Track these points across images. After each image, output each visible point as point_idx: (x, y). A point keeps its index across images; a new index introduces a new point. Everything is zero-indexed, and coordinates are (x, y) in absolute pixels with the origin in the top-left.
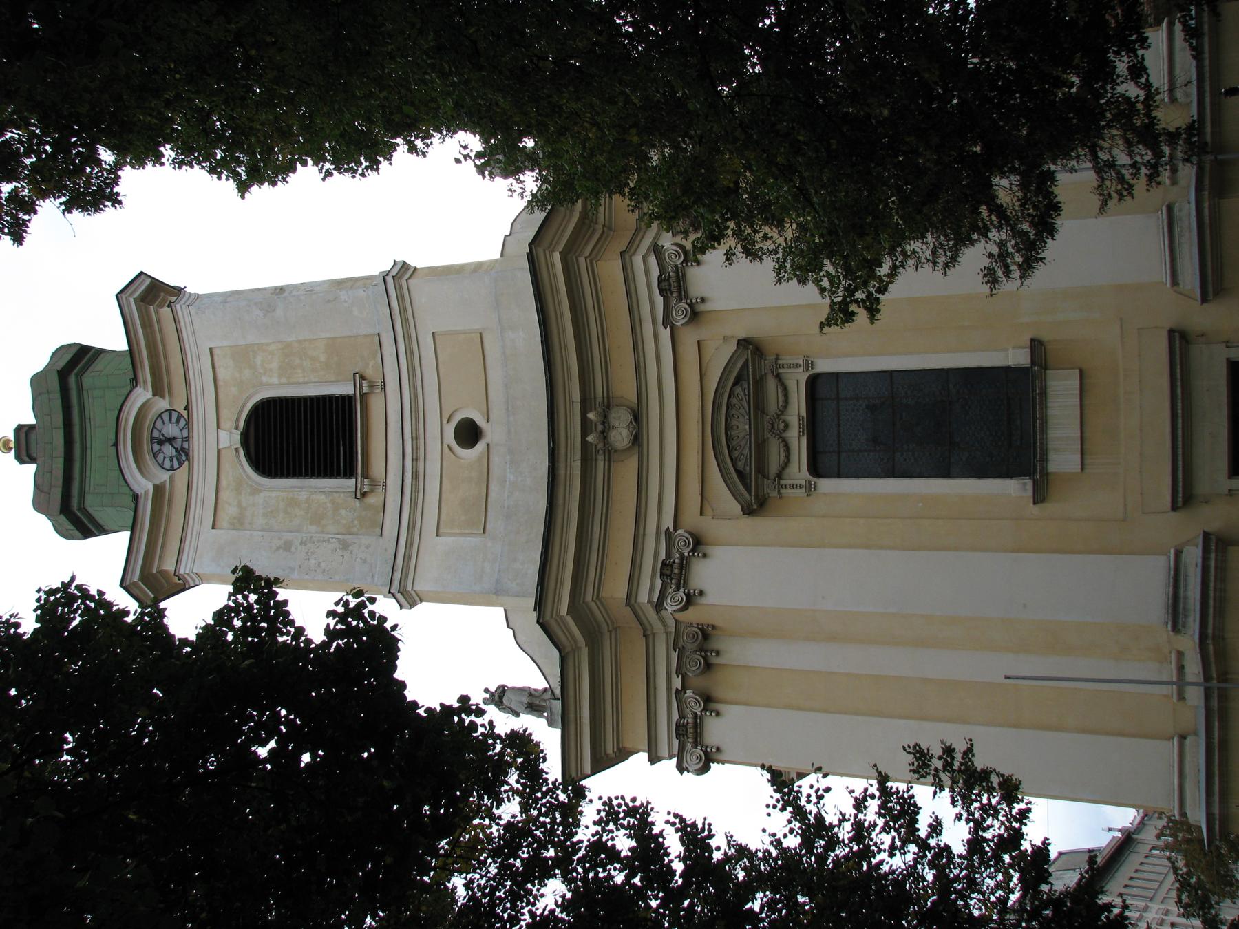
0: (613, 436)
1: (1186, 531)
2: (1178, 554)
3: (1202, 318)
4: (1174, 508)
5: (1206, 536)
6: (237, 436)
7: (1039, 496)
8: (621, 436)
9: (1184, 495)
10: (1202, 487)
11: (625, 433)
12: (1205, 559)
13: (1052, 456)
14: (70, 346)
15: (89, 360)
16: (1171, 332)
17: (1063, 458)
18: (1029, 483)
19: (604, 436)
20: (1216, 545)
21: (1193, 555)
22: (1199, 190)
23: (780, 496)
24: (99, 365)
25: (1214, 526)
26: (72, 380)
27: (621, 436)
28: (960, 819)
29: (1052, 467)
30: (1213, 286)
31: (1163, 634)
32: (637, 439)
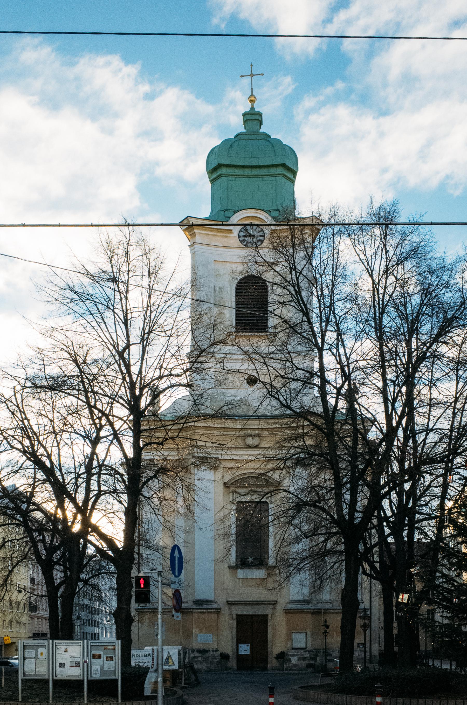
0: (250, 439)
1: (221, 601)
2: (215, 602)
3: (279, 609)
4: (227, 601)
5: (220, 609)
6: (254, 273)
7: (230, 567)
8: (250, 441)
9: (230, 603)
10: (233, 608)
11: (251, 443)
12: (214, 609)
13: (242, 571)
14: (297, 168)
15: (227, 236)
16: (276, 601)
17: (241, 573)
18: (234, 565)
19: (251, 436)
20: (218, 611)
21: (215, 606)
22: (314, 609)
23: (230, 493)
24: (292, 184)
25: (223, 611)
26: (280, 170)
27: (250, 441)
28: (220, 289)
29: (239, 570)
30: (287, 611)
31: (191, 598)
32: (249, 447)
